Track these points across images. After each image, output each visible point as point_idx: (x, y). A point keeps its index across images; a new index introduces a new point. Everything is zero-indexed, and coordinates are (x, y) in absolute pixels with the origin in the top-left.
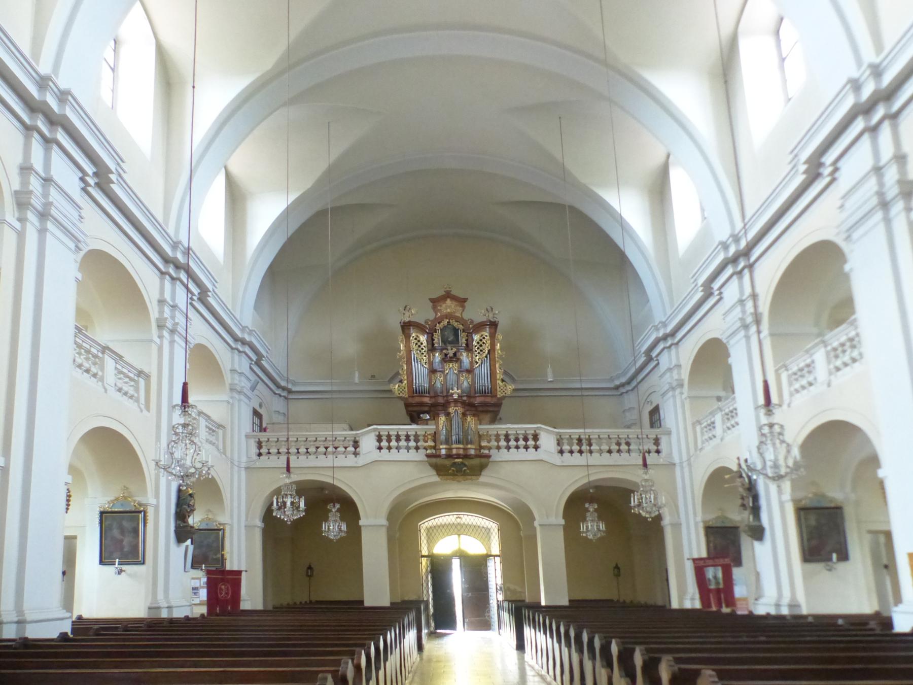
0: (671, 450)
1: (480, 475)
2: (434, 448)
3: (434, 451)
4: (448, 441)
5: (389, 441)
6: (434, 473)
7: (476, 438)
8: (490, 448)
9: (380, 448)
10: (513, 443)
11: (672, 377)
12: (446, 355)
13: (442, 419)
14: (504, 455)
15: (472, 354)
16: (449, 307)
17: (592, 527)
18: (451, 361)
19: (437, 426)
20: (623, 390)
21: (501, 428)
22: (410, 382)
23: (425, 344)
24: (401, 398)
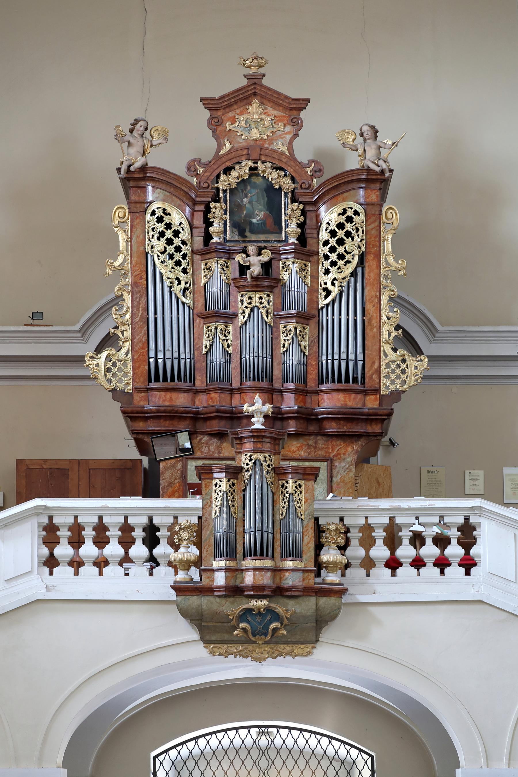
2: (198, 563)
3: (194, 574)
4: (228, 550)
5: (77, 542)
6: (195, 635)
9: (51, 563)
10: (406, 551)
12: (243, 269)
13: (221, 482)
14: (382, 585)
16: (254, 124)
18: (257, 285)
19: (207, 506)
21: (378, 509)
22: (141, 350)
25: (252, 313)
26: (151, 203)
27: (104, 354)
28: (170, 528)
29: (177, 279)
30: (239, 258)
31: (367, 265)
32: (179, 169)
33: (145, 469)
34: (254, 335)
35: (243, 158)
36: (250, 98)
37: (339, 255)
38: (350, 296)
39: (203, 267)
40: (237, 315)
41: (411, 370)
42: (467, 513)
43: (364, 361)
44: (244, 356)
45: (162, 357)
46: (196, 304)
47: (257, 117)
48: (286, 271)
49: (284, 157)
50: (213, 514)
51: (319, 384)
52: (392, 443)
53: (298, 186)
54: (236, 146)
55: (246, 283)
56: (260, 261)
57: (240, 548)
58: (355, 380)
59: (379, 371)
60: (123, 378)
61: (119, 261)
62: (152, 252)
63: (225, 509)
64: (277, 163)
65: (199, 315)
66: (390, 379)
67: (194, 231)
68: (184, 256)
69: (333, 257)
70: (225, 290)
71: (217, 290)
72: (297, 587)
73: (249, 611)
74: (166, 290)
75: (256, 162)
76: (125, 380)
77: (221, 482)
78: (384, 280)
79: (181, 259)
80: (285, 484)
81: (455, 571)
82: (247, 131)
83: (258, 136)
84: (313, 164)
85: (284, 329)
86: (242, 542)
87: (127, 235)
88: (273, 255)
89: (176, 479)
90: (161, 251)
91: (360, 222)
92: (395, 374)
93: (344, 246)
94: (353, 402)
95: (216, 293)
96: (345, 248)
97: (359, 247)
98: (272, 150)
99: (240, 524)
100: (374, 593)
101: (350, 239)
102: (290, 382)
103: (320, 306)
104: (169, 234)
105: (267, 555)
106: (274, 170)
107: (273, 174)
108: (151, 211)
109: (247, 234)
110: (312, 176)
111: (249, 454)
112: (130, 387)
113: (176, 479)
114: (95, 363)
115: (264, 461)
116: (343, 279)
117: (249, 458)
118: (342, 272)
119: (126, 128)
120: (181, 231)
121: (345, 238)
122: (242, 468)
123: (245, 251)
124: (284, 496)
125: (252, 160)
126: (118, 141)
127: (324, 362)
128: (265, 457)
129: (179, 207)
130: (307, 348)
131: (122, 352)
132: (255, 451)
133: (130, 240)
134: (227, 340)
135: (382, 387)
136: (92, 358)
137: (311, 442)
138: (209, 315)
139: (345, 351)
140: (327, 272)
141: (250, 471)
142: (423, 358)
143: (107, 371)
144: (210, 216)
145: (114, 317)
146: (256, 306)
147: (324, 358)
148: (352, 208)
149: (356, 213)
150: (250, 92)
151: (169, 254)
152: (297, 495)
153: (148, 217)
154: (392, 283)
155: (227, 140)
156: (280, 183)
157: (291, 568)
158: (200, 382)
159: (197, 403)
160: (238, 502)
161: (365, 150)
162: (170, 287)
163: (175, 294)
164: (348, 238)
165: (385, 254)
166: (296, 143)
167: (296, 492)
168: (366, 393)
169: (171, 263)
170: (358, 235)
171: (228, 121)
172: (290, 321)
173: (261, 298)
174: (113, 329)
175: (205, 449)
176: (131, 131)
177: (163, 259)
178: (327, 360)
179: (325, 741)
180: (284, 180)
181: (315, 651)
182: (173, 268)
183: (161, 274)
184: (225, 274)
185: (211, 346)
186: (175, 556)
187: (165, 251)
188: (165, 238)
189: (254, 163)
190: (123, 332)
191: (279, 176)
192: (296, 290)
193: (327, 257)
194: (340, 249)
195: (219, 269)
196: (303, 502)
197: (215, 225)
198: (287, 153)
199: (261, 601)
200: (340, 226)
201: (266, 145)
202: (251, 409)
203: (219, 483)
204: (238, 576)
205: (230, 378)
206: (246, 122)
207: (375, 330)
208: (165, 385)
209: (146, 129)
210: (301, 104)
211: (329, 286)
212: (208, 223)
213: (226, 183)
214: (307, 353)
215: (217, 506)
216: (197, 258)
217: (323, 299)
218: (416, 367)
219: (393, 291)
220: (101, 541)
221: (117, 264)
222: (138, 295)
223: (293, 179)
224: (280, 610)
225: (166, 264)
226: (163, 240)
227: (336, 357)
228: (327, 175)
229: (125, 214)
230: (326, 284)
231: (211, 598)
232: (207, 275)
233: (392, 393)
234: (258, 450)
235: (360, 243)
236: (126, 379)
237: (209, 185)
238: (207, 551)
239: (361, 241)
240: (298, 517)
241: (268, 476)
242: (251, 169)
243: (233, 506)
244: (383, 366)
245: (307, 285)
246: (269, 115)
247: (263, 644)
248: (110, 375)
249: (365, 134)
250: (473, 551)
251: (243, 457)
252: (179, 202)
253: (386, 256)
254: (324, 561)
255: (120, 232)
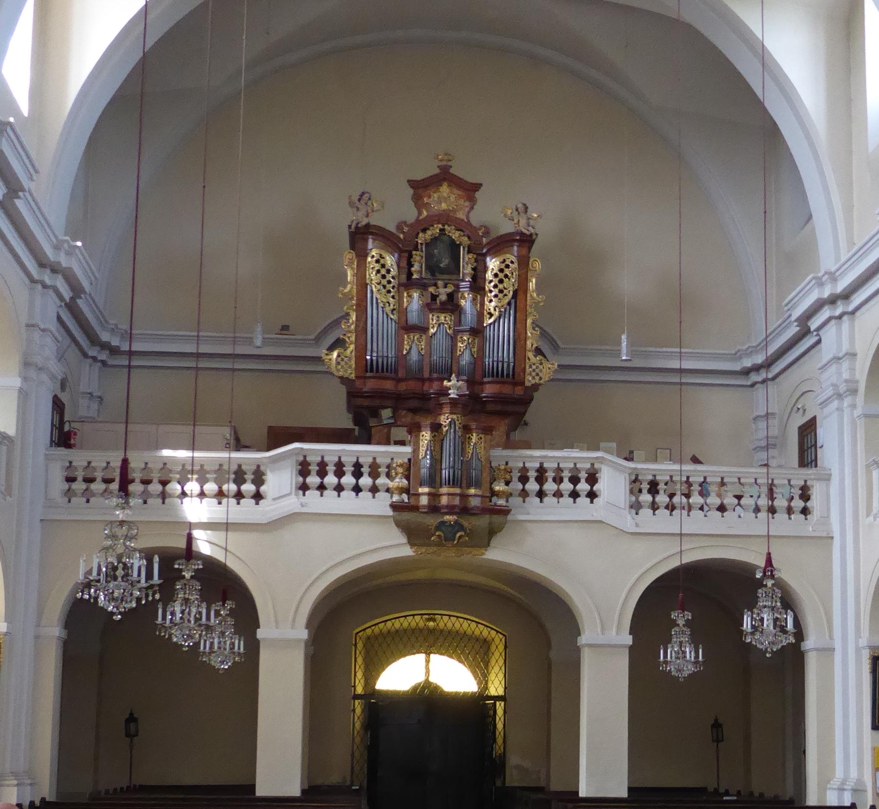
0: (829, 510)
2: (406, 491)
3: (405, 497)
4: (433, 480)
5: (322, 473)
6: (403, 540)
7: (486, 477)
8: (508, 495)
9: (304, 488)
10: (550, 486)
11: (839, 373)
12: (434, 297)
13: (426, 436)
15: (484, 295)
16: (444, 199)
17: (681, 656)
19: (416, 451)
20: (754, 377)
21: (534, 457)
22: (361, 350)
23: (394, 272)
27: (335, 354)
28: (388, 467)
30: (431, 289)
32: (391, 227)
43: (514, 363)
72: (478, 507)
73: (443, 523)
74: (380, 309)
75: (444, 226)
81: (583, 500)
94: (507, 390)
104: (383, 271)
109: (437, 274)
119: (355, 198)
123: (435, 285)
133: (355, 275)
138: (409, 328)
140: (491, 301)
149: (512, 262)
153: (369, 259)
158: (401, 374)
166: (471, 215)
168: (515, 384)
176: (359, 200)
179: (473, 625)
185: (410, 349)
186: (391, 484)
191: (460, 236)
194: (501, 286)
210: (477, 187)
211: (492, 310)
212: (410, 265)
220: (340, 473)
221: (346, 291)
223: (469, 238)
224: (465, 524)
242: (440, 230)
244: (527, 367)
248: (339, 367)
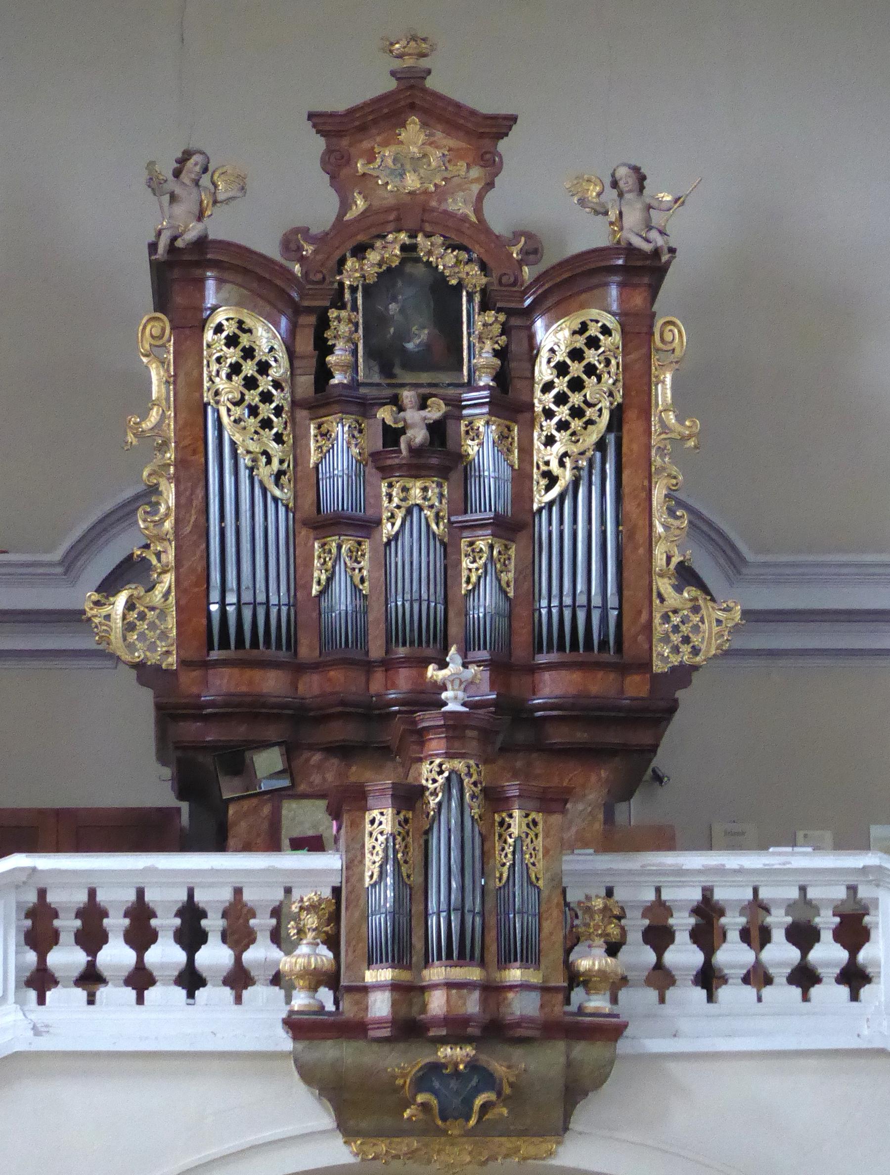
1: (562, 1129)
4: (401, 948)
6: (325, 1120)
8: (617, 984)
9: (41, 981)
10: (733, 955)
12: (392, 435)
13: (381, 821)
16: (411, 162)
19: (353, 864)
21: (684, 872)
22: (193, 588)
24: (145, 673)
25: (408, 519)
26: (214, 309)
27: (121, 600)
29: (265, 453)
30: (385, 414)
31: (625, 428)
32: (268, 246)
33: (182, 829)
34: (414, 558)
35: (390, 227)
36: (403, 116)
37: (572, 409)
38: (593, 488)
39: (313, 432)
40: (379, 522)
41: (710, 628)
42: (852, 880)
43: (620, 608)
44: (393, 599)
45: (234, 600)
46: (299, 501)
47: (416, 150)
48: (473, 440)
49: (467, 225)
50: (367, 879)
51: (534, 654)
52: (658, 778)
53: (494, 279)
54: (376, 203)
55: (397, 461)
56: (425, 418)
57: (418, 944)
58: (604, 644)
59: (649, 627)
60: (158, 642)
61: (153, 419)
62: (217, 402)
63: (389, 868)
64: (453, 237)
65: (306, 523)
66: (671, 645)
67: (297, 363)
68: (278, 411)
69: (562, 413)
70: (356, 476)
71: (340, 474)
73: (435, 1068)
74: (244, 474)
75: (413, 236)
76: (161, 648)
77: (381, 821)
78: (658, 458)
79: (272, 417)
80: (507, 819)
81: (829, 993)
82: (396, 177)
83: (419, 186)
84: (523, 239)
85: (469, 549)
86: (422, 932)
87: (168, 371)
88: (449, 408)
89: (258, 835)
90: (234, 400)
91: (612, 347)
92: (680, 634)
93: (583, 393)
94: (600, 685)
95: (340, 480)
96: (585, 396)
97: (611, 394)
98: (445, 212)
99: (419, 896)
100: (675, 1036)
101: (594, 379)
102: (479, 649)
103: (535, 507)
104: (249, 369)
105: (472, 958)
106: (449, 251)
107: (447, 259)
108: (213, 325)
109: (397, 370)
110: (521, 263)
111: (438, 761)
112: (172, 659)
113: (258, 835)
114: (104, 614)
115: (466, 775)
116: (582, 453)
117: (438, 769)
118: (578, 441)
119: (166, 169)
120: (273, 363)
121: (584, 377)
122: (424, 789)
123: (395, 401)
124: (505, 842)
125: (407, 231)
126: (153, 189)
127: (544, 611)
128: (468, 767)
129: (269, 318)
130: (512, 584)
131: (157, 592)
132: (449, 756)
133: (173, 381)
134: (360, 570)
135: (654, 659)
136: (97, 603)
137: (519, 764)
138: (324, 523)
139: (585, 589)
140: (550, 441)
141: (440, 795)
142: (732, 605)
143: (126, 629)
144: (328, 334)
145: (142, 526)
146: (417, 505)
147: (544, 603)
148: (597, 322)
149: (606, 331)
150: (402, 103)
151: (250, 407)
152: (529, 840)
153: (209, 335)
154: (674, 463)
155: (360, 193)
156: (460, 275)
157: (519, 983)
158: (307, 650)
159: (301, 687)
160: (415, 854)
161: (621, 213)
162: (251, 469)
163: (261, 482)
164: (590, 378)
165: (660, 408)
167: (527, 835)
168: (623, 669)
169: (252, 423)
170: (609, 373)
171: (361, 157)
172: (480, 533)
173: (425, 489)
174: (140, 548)
175: (316, 779)
176: (177, 174)
177: (237, 416)
178: (549, 607)
180: (467, 268)
181: (561, 1149)
182: (256, 432)
183: (233, 444)
184: (356, 445)
185: (330, 580)
186: (286, 963)
187: (242, 400)
188: (242, 375)
189: (410, 237)
190: (158, 555)
191: (458, 262)
192: (492, 474)
193: (549, 414)
194: (576, 399)
195: (346, 436)
196: (540, 855)
197: (337, 352)
198: (473, 219)
199: (461, 1048)
200: (576, 354)
201: (434, 204)
202: (442, 674)
203: (378, 818)
204: (415, 1000)
205: (366, 643)
206: (395, 160)
207: (641, 551)
208: (241, 654)
209: (205, 170)
210: (500, 126)
211: (554, 467)
212: (324, 348)
213: (357, 275)
214: (511, 594)
215: (374, 863)
216: (302, 414)
217: (543, 492)
218: (719, 622)
219: (675, 478)
220: (141, 936)
221: (147, 425)
222: (190, 484)
223: (484, 267)
224: (499, 1068)
225: (242, 423)
226: (237, 380)
227: (567, 601)
228: (550, 259)
229: (163, 330)
230: (547, 463)
231: (361, 1044)
232: (320, 447)
233: (673, 669)
234: (455, 753)
235: (613, 388)
236: (163, 644)
237: (324, 278)
238: (354, 951)
239: (614, 384)
240: (532, 883)
241: (475, 803)
243: (406, 862)
244: (657, 620)
245: (512, 466)
246: (437, 147)
247: (463, 1136)
249: (621, 184)
250: (863, 956)
251: (425, 767)
252: (268, 308)
253: (661, 412)
254: (582, 969)
255: (154, 365)
